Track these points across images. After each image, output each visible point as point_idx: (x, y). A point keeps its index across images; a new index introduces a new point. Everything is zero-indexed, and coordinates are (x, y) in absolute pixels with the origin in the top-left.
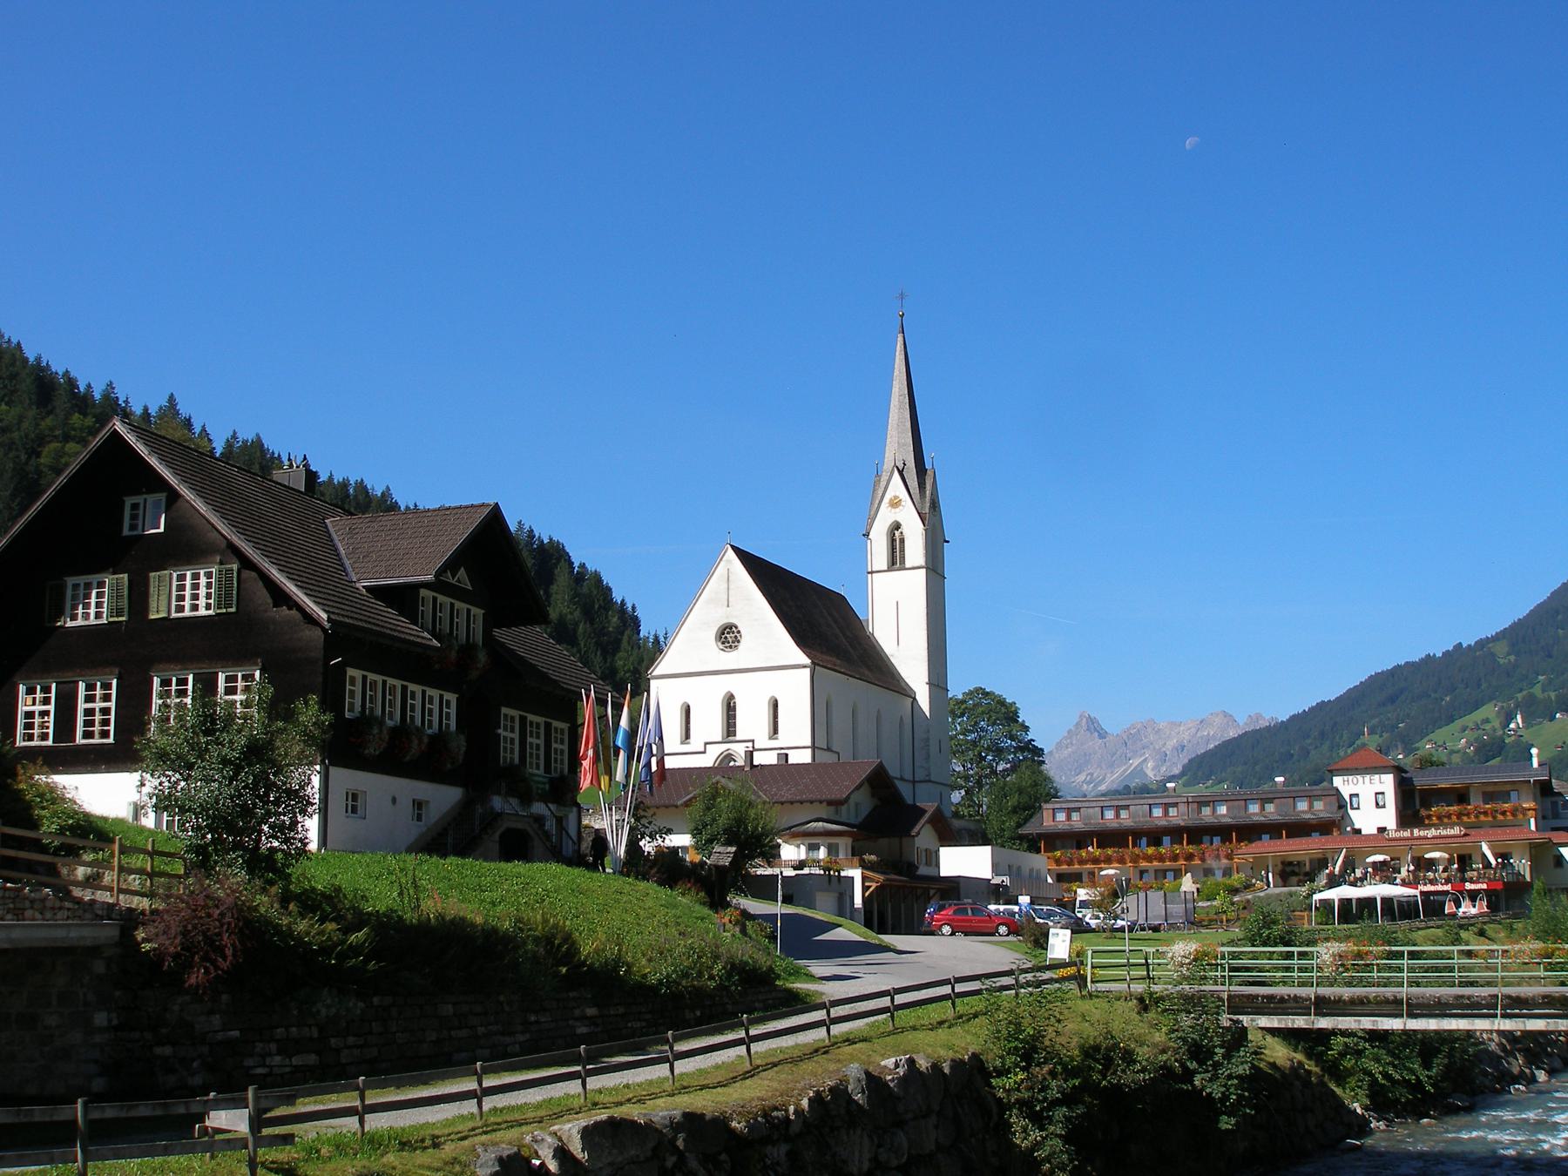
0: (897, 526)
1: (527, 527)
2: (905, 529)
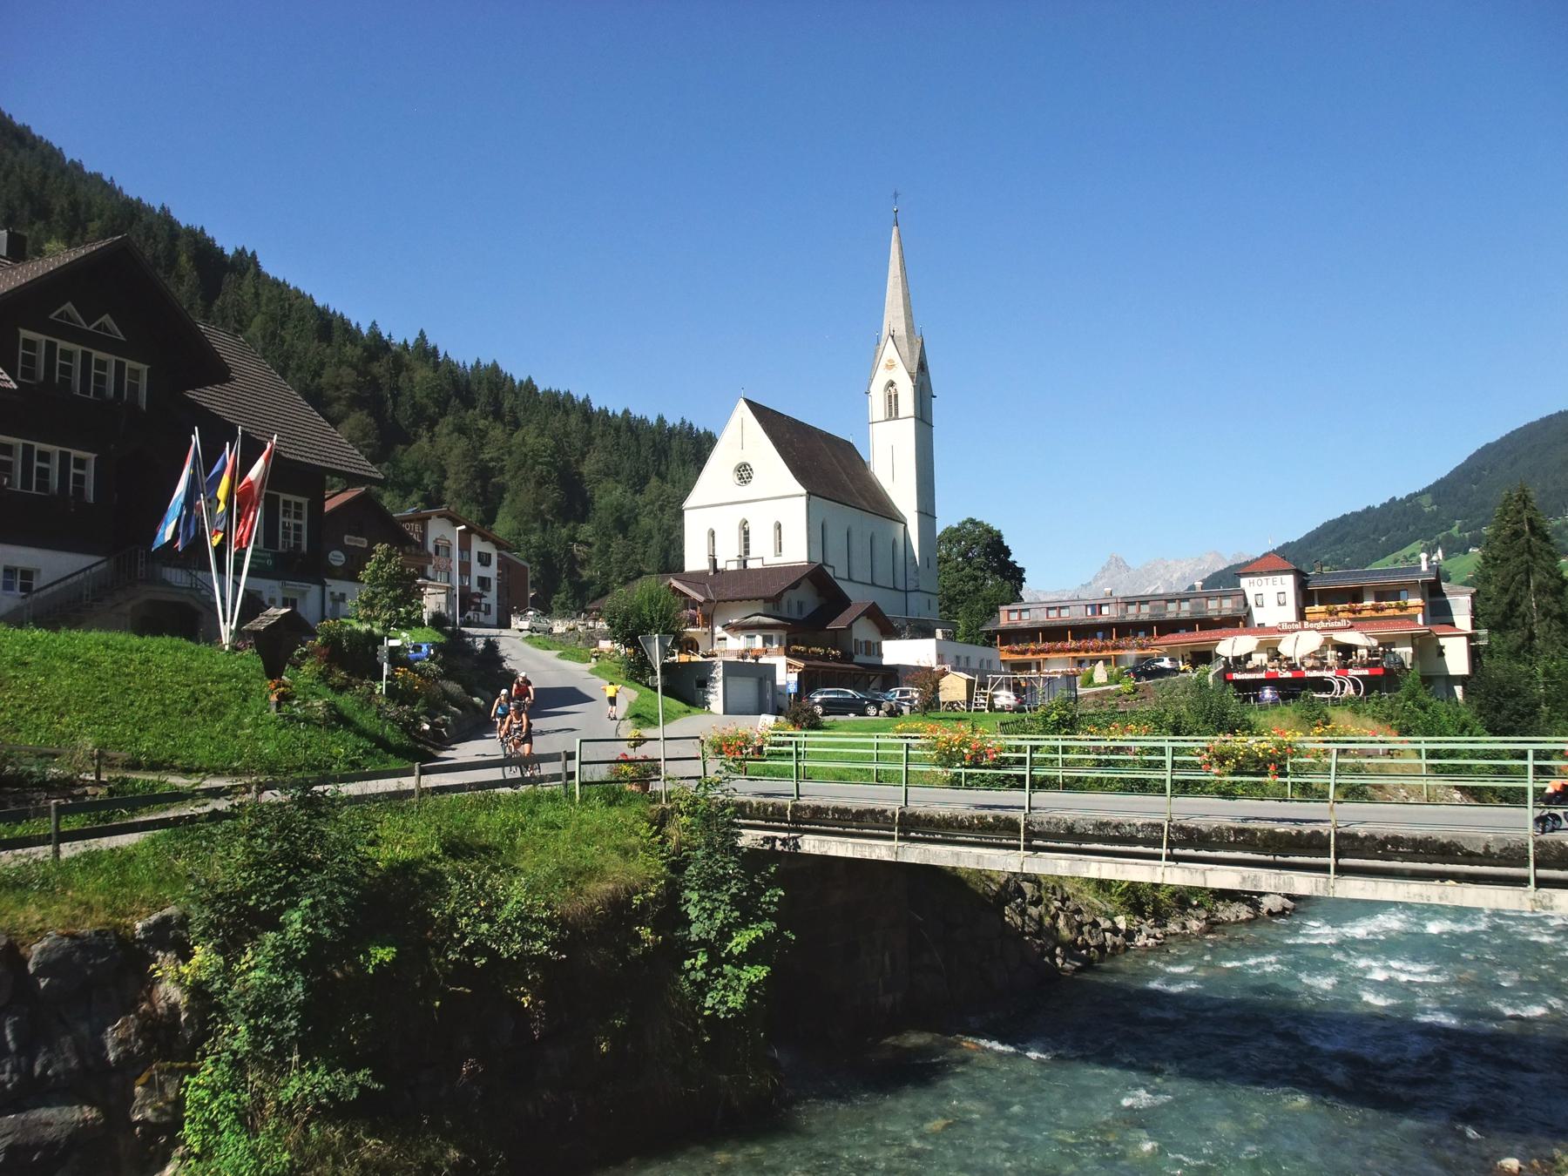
0: (892, 384)
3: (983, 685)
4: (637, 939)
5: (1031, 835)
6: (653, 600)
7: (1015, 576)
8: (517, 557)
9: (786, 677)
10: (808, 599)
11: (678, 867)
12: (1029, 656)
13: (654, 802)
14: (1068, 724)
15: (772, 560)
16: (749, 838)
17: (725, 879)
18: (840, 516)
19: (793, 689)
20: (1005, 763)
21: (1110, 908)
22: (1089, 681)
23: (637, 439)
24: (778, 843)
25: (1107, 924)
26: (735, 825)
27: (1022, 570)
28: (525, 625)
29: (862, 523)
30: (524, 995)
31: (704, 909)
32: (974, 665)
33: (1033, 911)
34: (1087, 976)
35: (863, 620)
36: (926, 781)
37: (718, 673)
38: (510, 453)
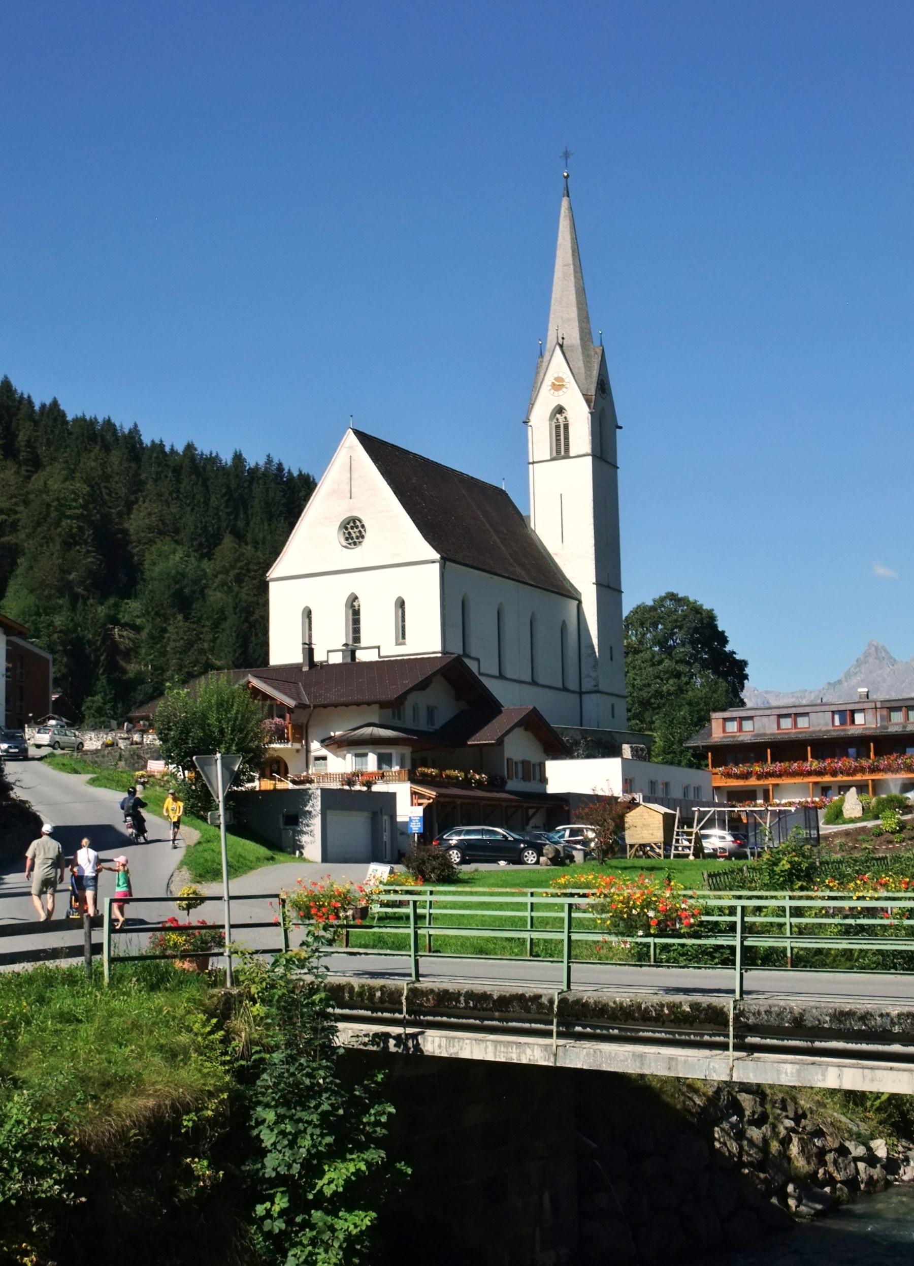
0: (560, 410)
1: (276, 461)
2: (570, 414)
3: (687, 821)
4: (189, 1175)
5: (743, 1029)
6: (223, 705)
7: (734, 672)
8: (35, 645)
9: (409, 811)
10: (442, 705)
11: (246, 1075)
12: (753, 782)
13: (214, 985)
14: (802, 876)
15: (391, 650)
16: (348, 1035)
17: (314, 1092)
18: (490, 592)
19: (416, 827)
20: (714, 929)
21: (864, 1128)
22: (837, 816)
23: (205, 485)
24: (392, 1042)
25: (860, 1151)
26: (327, 1017)
27: (743, 664)
28: (44, 738)
29: (515, 598)
30: (26, 1253)
31: (283, 1133)
32: (676, 793)
33: (755, 1133)
34: (834, 1224)
35: (519, 731)
36: (601, 955)
37: (315, 805)
38: (26, 503)
